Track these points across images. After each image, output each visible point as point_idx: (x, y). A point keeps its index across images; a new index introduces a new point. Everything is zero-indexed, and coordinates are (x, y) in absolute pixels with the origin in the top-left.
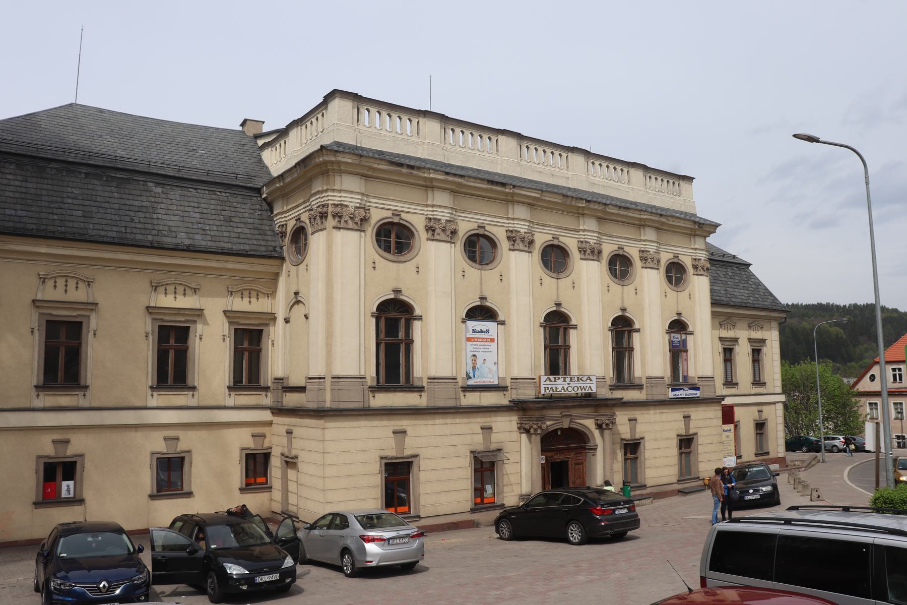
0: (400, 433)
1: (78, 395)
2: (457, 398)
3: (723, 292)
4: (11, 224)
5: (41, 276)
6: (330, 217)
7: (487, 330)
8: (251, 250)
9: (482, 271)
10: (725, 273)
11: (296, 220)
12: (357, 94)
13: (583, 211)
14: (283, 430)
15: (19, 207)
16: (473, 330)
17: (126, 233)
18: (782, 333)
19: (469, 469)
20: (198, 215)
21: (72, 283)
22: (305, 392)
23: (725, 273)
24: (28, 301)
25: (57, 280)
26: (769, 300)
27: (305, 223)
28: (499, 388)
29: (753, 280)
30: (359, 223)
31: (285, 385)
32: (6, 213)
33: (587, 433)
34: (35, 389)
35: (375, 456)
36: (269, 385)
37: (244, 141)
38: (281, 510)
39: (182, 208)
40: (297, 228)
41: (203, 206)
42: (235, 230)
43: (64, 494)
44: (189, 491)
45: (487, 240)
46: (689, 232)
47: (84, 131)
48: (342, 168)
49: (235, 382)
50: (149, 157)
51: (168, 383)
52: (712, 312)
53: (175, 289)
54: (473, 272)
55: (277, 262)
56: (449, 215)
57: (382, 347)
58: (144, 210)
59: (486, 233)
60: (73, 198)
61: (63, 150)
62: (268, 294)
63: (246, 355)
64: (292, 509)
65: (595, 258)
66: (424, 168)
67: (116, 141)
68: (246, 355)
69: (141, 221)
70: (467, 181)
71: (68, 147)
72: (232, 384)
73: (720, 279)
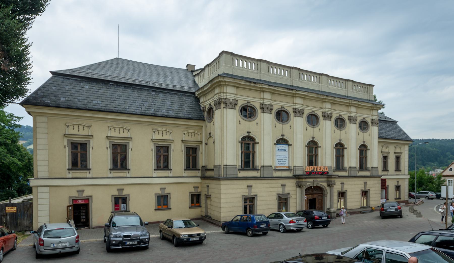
0: (250, 187)
1: (126, 172)
2: (272, 174)
3: (384, 133)
4: (96, 107)
5: (109, 127)
6: (222, 104)
7: (285, 149)
8: (192, 117)
9: (283, 125)
10: (385, 125)
11: (209, 105)
12: (232, 53)
13: (325, 100)
14: (205, 185)
15: (98, 100)
16: (278, 149)
17: (142, 110)
18: (410, 150)
19: (276, 201)
20: (170, 103)
21: (121, 130)
22: (213, 171)
23: (385, 125)
24: (105, 137)
25: (116, 129)
26: (405, 137)
27: (213, 106)
28: (289, 170)
29: (398, 128)
30: (234, 106)
31: (206, 168)
32: (94, 102)
33: (324, 188)
34: (68, 170)
35: (240, 195)
38: (205, 215)
39: (164, 100)
40: (210, 108)
41: (171, 99)
42: (185, 109)
45: (286, 113)
46: (371, 108)
48: (227, 84)
49: (187, 168)
51: (250, 167)
52: (379, 141)
53: (162, 132)
54: (279, 125)
56: (301, 107)
57: (243, 154)
58: (149, 101)
59: (285, 110)
60: (120, 96)
61: (114, 77)
62: (199, 134)
63: (162, 157)
64: (209, 214)
65: (329, 119)
66: (260, 83)
68: (162, 157)
69: (148, 106)
70: (277, 88)
71: (116, 76)
72: (186, 168)
73: (383, 128)
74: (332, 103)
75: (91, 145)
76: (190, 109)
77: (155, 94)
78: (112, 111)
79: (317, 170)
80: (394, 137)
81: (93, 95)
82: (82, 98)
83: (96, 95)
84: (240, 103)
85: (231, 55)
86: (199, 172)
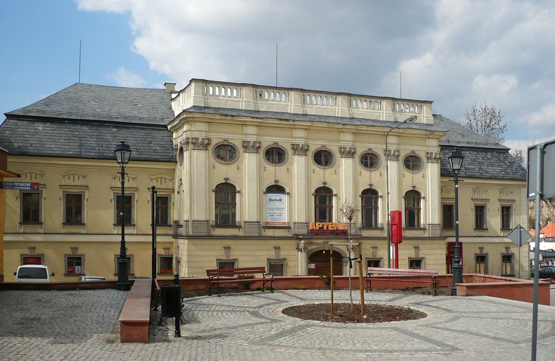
0: (227, 248)
4: (49, 152)
9: (276, 167)
15: (52, 143)
16: (269, 199)
20: (135, 142)
36: (172, 224)
37: (164, 96)
42: (153, 148)
43: (77, 272)
44: (133, 273)
47: (81, 100)
49: (476, 227)
50: (112, 111)
55: (174, 164)
58: (108, 140)
67: (97, 104)
72: (475, 228)
74: (354, 133)
75: (44, 195)
76: (159, 148)
77: (117, 131)
78: (66, 156)
79: (327, 228)
80: (496, 175)
81: (47, 137)
82: (36, 142)
83: (49, 137)
84: (404, 154)
85: (203, 83)
86: (170, 229)
